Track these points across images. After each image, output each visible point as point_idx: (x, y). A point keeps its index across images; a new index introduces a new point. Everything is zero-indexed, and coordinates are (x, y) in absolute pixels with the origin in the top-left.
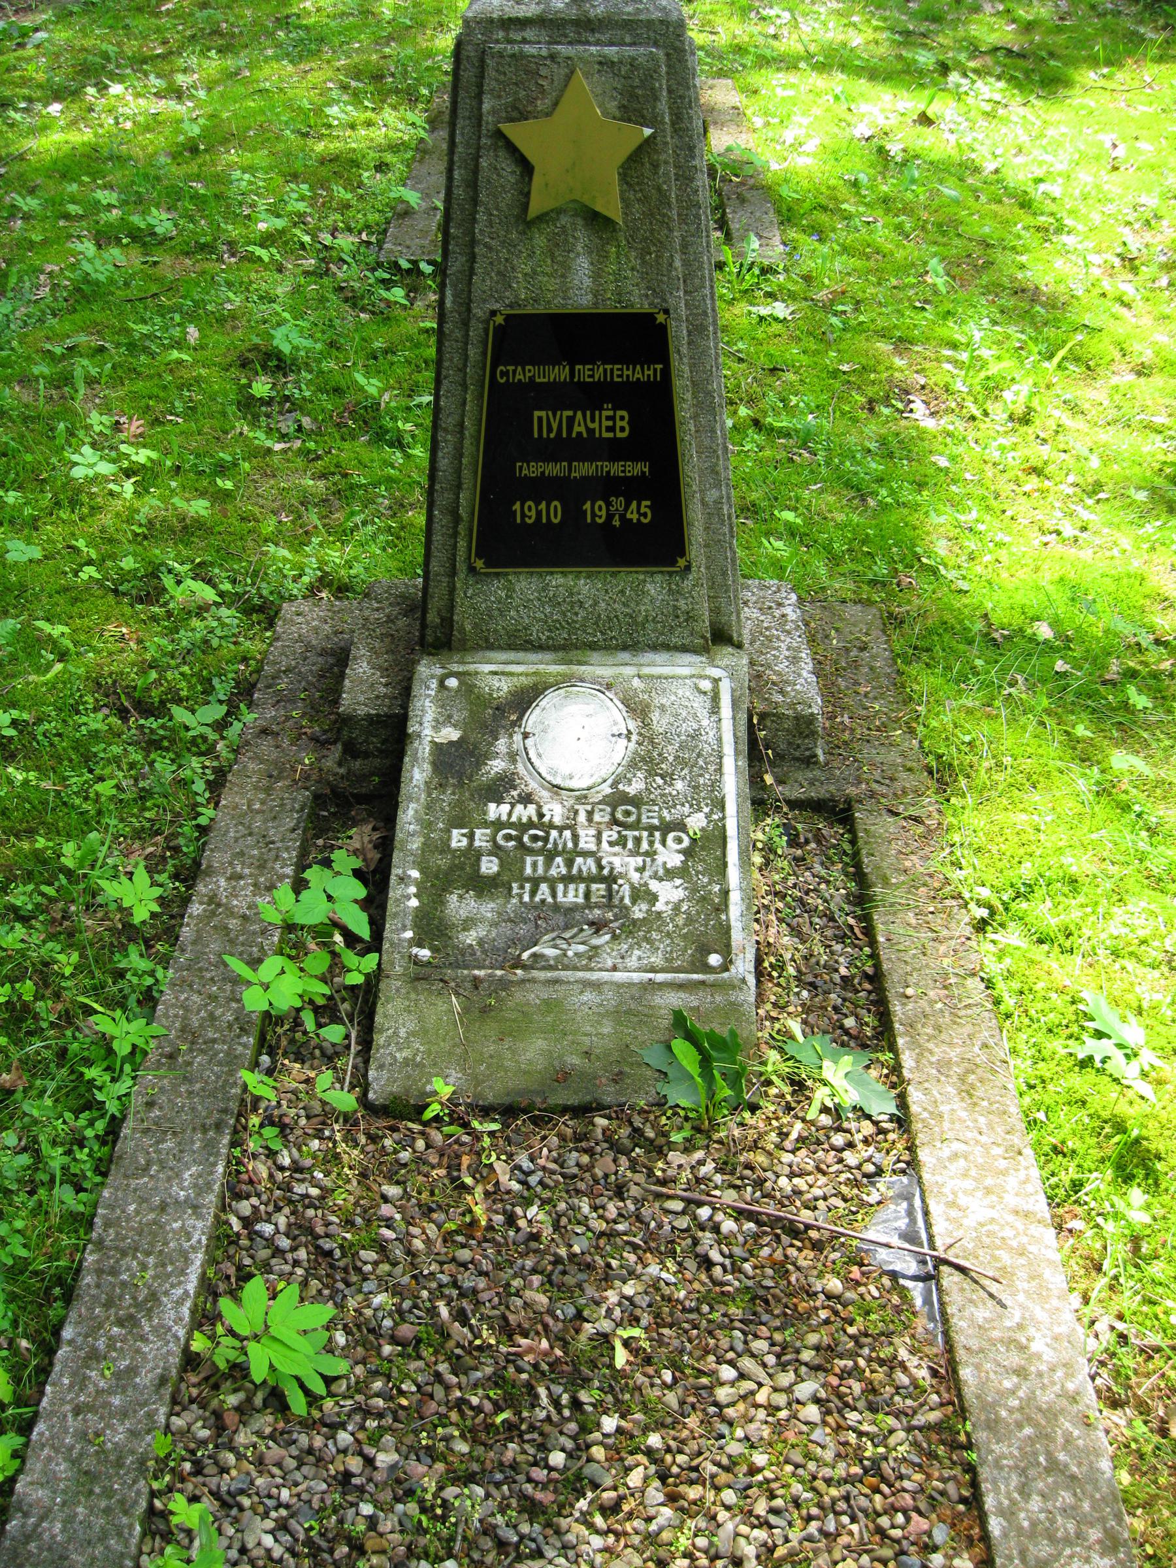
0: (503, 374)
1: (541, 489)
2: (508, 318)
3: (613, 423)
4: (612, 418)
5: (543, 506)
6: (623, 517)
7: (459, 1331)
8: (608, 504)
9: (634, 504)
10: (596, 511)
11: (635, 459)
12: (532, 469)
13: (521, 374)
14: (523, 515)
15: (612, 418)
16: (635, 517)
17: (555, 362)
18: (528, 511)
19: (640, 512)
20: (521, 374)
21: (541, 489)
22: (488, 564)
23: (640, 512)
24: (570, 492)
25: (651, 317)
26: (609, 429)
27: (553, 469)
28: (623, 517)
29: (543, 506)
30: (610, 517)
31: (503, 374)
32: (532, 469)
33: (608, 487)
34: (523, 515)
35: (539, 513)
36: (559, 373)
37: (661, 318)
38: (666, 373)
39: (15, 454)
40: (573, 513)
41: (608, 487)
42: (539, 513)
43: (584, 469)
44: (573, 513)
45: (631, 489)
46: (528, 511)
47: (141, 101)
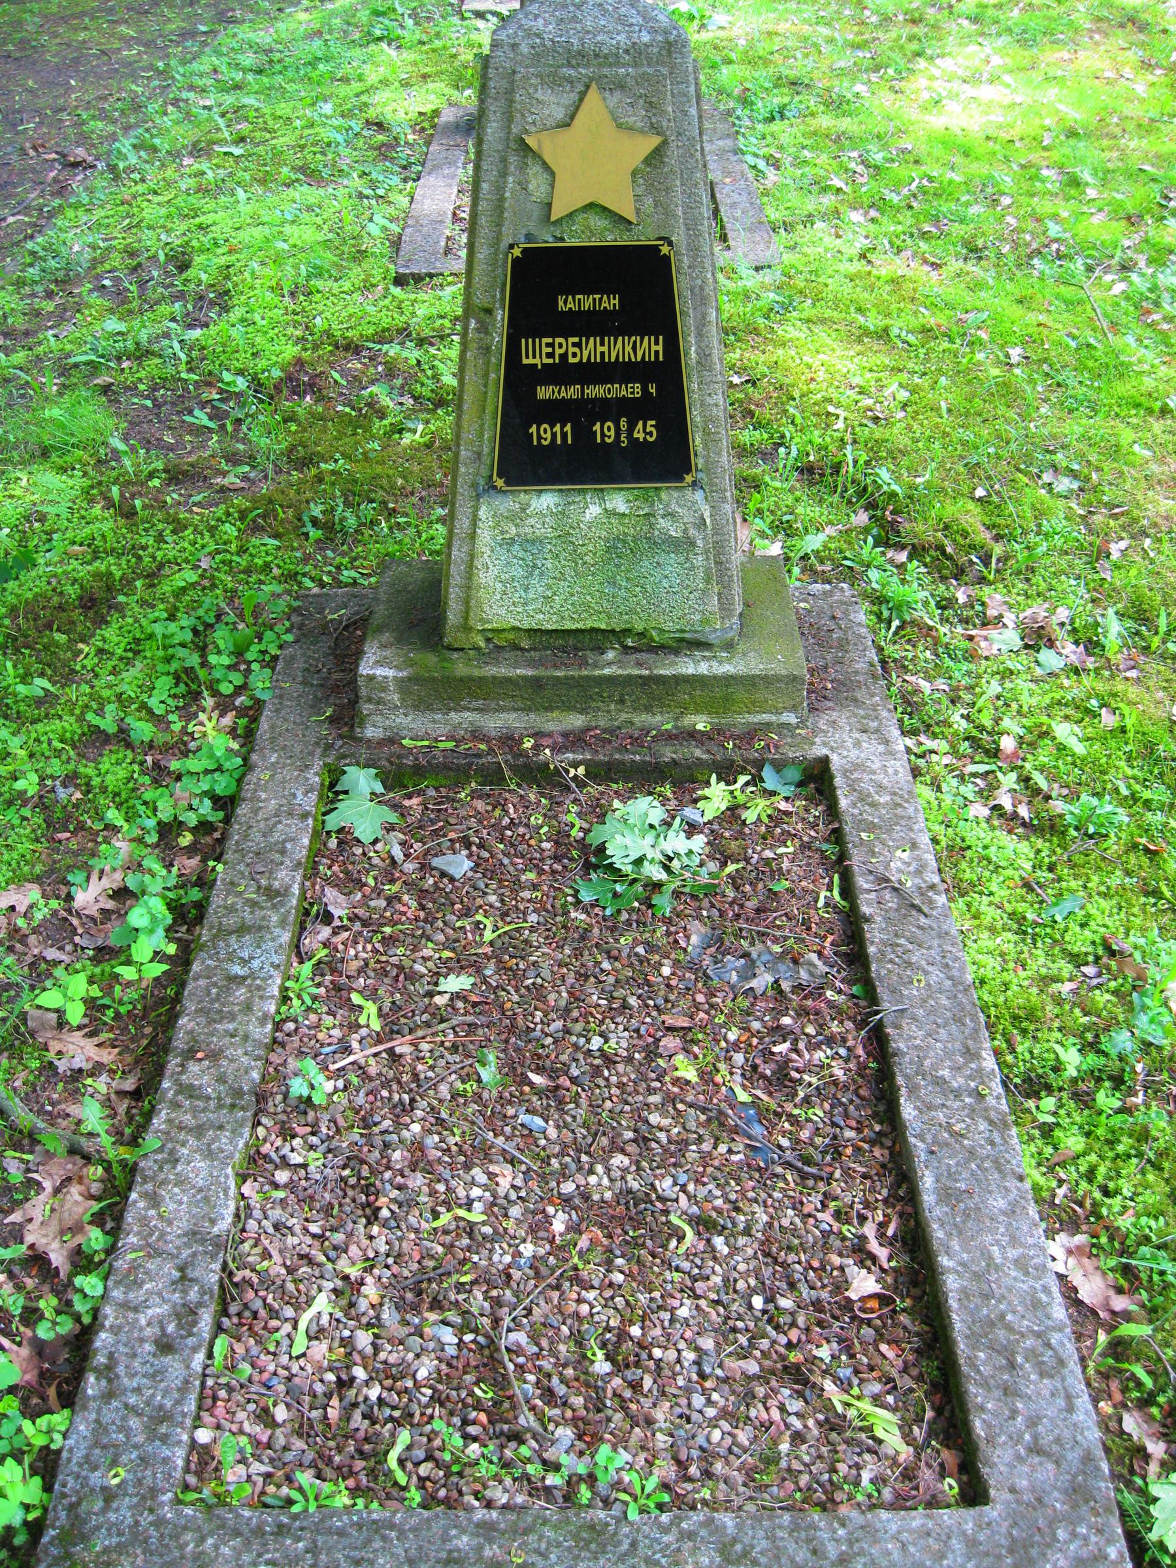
1: (555, 412)
2: (667, 258)
4: (551, 345)
5: (557, 428)
7: (553, 1480)
9: (640, 424)
10: (606, 432)
15: (551, 345)
16: (641, 436)
18: (544, 434)
19: (646, 431)
21: (555, 412)
22: (507, 483)
23: (646, 431)
24: (582, 414)
25: (656, 249)
26: (549, 355)
27: (571, 392)
29: (557, 428)
34: (603, 435)
35: (554, 435)
37: (665, 250)
40: (583, 433)
42: (554, 435)
43: (596, 391)
44: (583, 433)
45: (633, 410)
46: (544, 434)
47: (122, 1149)
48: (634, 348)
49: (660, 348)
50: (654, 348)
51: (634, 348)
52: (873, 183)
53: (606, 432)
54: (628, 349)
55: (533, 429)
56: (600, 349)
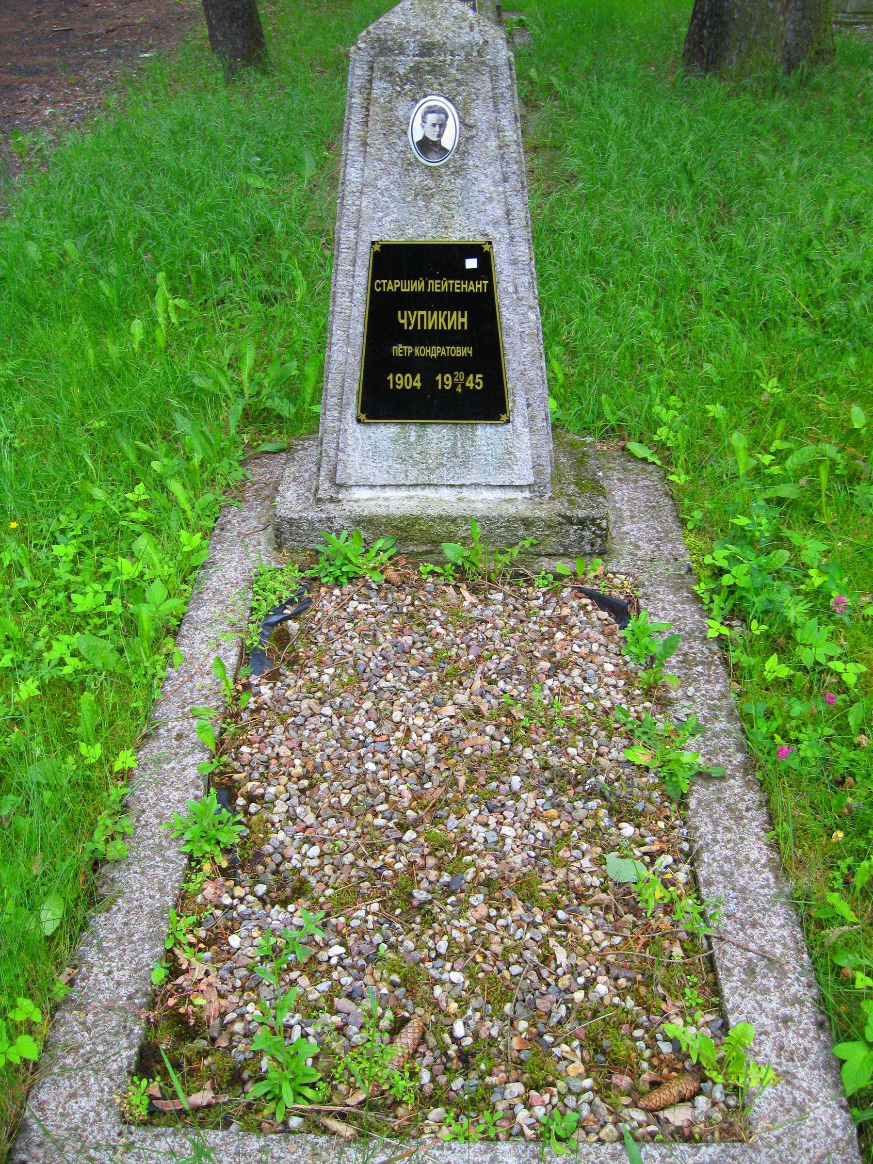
0: (379, 285)
1: (407, 365)
3: (458, 320)
6: (463, 385)
8: (453, 377)
9: (471, 377)
10: (445, 381)
11: (462, 344)
12: (398, 350)
13: (391, 286)
14: (443, 383)
16: (471, 385)
17: (414, 278)
19: (475, 382)
20: (391, 286)
21: (407, 365)
23: (475, 382)
24: (429, 368)
28: (463, 385)
30: (455, 385)
31: (379, 285)
32: (398, 350)
33: (449, 365)
34: (443, 383)
36: (417, 286)
38: (491, 286)
39: (528, 1087)
40: (429, 382)
41: (449, 365)
43: (435, 352)
44: (429, 382)
48: (446, 320)
49: (465, 320)
50: (461, 320)
51: (446, 320)
52: (418, 137)
53: (445, 381)
54: (442, 320)
55: (439, 377)
56: (461, 320)
